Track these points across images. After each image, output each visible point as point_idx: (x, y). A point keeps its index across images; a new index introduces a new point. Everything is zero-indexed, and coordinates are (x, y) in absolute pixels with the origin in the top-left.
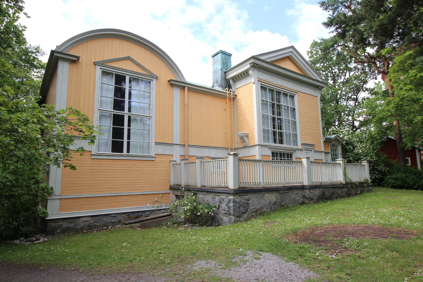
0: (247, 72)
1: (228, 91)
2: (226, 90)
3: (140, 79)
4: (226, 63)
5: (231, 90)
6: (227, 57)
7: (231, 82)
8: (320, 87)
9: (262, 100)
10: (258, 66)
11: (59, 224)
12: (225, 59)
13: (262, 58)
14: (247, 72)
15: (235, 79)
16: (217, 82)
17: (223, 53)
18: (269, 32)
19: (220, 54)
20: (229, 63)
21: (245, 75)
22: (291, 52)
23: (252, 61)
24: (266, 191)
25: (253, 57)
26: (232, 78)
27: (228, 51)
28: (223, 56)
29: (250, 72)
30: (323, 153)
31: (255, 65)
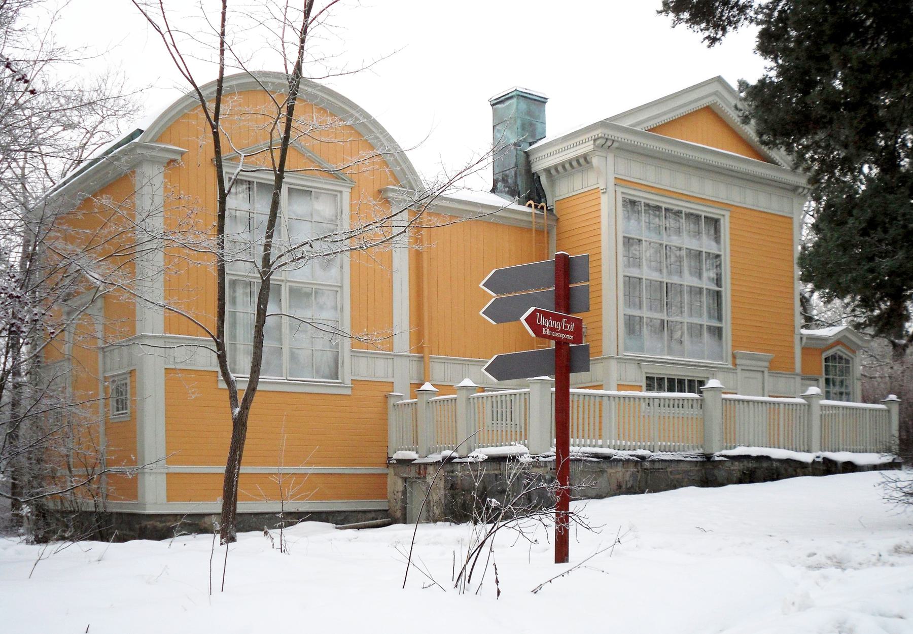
0: (586, 159)
1: (536, 207)
2: (530, 206)
3: (313, 190)
4: (531, 124)
5: (543, 204)
6: (533, 107)
7: (543, 180)
8: (800, 190)
9: (624, 237)
10: (616, 145)
11: (168, 524)
12: (529, 113)
13: (626, 123)
14: (586, 159)
15: (553, 172)
16: (504, 180)
17: (523, 96)
18: (438, 523)
19: (514, 101)
20: (539, 125)
21: (582, 163)
22: (716, 93)
23: (599, 132)
24: (277, 209)
25: (603, 124)
26: (548, 171)
27: (536, 89)
28: (523, 105)
29: (595, 161)
30: (798, 379)
31: (609, 143)
